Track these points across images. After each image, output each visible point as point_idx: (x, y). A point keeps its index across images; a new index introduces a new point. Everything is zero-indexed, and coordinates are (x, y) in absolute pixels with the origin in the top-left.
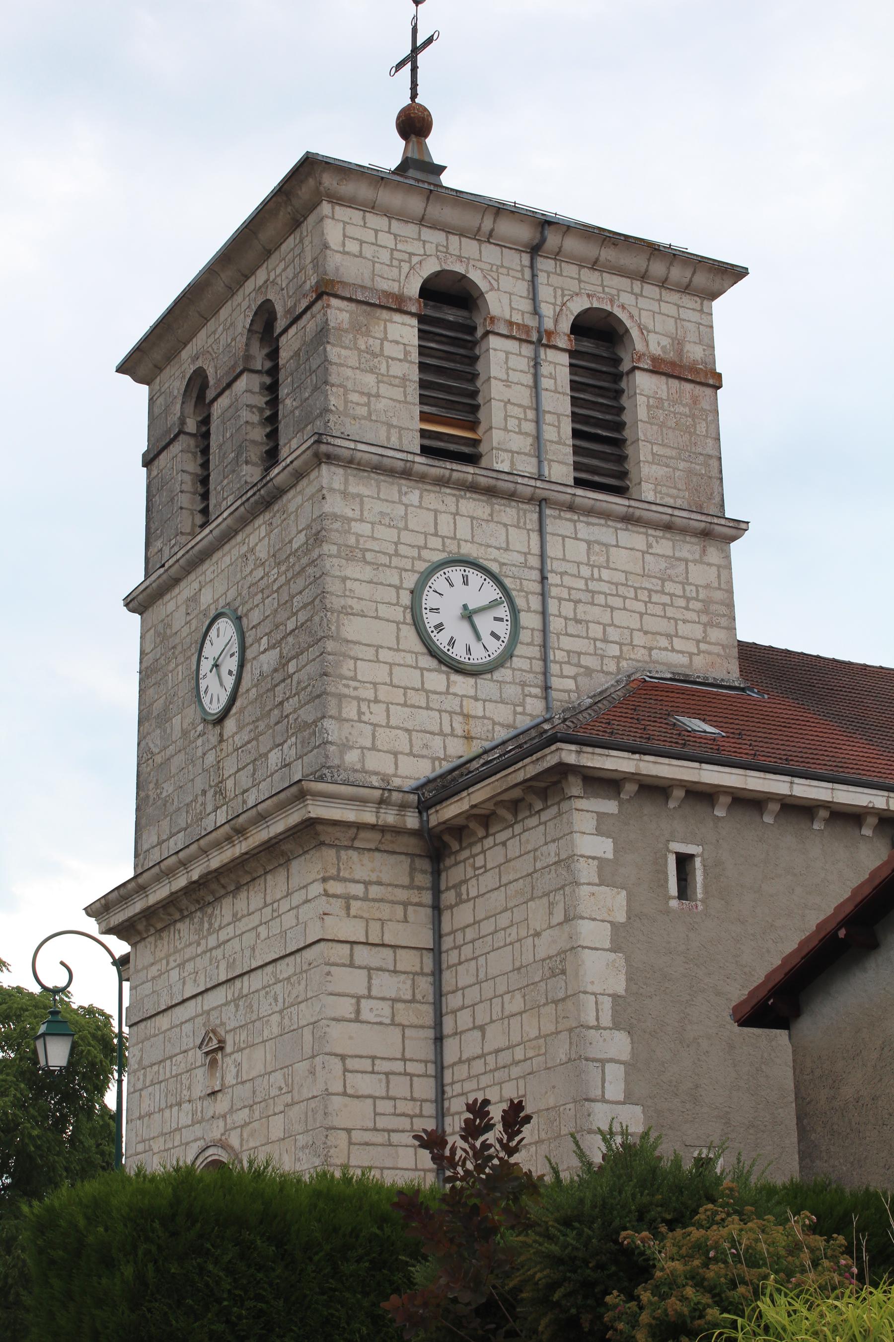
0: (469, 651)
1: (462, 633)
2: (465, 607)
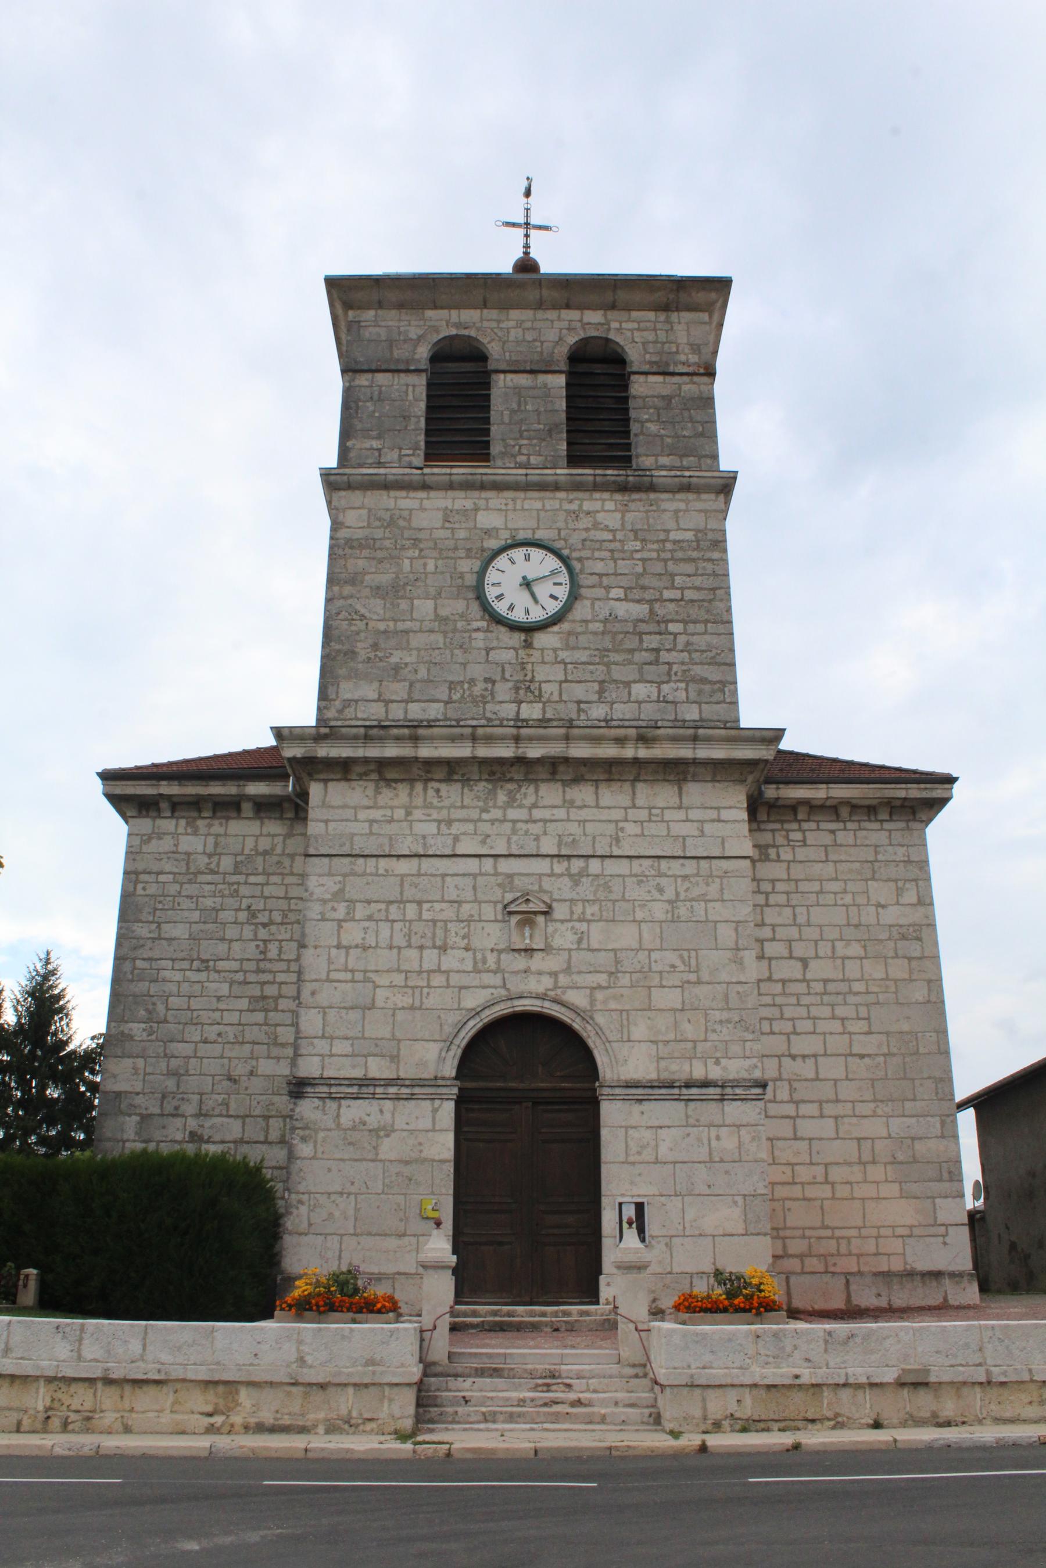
0: (527, 612)
1: (522, 599)
2: (524, 578)
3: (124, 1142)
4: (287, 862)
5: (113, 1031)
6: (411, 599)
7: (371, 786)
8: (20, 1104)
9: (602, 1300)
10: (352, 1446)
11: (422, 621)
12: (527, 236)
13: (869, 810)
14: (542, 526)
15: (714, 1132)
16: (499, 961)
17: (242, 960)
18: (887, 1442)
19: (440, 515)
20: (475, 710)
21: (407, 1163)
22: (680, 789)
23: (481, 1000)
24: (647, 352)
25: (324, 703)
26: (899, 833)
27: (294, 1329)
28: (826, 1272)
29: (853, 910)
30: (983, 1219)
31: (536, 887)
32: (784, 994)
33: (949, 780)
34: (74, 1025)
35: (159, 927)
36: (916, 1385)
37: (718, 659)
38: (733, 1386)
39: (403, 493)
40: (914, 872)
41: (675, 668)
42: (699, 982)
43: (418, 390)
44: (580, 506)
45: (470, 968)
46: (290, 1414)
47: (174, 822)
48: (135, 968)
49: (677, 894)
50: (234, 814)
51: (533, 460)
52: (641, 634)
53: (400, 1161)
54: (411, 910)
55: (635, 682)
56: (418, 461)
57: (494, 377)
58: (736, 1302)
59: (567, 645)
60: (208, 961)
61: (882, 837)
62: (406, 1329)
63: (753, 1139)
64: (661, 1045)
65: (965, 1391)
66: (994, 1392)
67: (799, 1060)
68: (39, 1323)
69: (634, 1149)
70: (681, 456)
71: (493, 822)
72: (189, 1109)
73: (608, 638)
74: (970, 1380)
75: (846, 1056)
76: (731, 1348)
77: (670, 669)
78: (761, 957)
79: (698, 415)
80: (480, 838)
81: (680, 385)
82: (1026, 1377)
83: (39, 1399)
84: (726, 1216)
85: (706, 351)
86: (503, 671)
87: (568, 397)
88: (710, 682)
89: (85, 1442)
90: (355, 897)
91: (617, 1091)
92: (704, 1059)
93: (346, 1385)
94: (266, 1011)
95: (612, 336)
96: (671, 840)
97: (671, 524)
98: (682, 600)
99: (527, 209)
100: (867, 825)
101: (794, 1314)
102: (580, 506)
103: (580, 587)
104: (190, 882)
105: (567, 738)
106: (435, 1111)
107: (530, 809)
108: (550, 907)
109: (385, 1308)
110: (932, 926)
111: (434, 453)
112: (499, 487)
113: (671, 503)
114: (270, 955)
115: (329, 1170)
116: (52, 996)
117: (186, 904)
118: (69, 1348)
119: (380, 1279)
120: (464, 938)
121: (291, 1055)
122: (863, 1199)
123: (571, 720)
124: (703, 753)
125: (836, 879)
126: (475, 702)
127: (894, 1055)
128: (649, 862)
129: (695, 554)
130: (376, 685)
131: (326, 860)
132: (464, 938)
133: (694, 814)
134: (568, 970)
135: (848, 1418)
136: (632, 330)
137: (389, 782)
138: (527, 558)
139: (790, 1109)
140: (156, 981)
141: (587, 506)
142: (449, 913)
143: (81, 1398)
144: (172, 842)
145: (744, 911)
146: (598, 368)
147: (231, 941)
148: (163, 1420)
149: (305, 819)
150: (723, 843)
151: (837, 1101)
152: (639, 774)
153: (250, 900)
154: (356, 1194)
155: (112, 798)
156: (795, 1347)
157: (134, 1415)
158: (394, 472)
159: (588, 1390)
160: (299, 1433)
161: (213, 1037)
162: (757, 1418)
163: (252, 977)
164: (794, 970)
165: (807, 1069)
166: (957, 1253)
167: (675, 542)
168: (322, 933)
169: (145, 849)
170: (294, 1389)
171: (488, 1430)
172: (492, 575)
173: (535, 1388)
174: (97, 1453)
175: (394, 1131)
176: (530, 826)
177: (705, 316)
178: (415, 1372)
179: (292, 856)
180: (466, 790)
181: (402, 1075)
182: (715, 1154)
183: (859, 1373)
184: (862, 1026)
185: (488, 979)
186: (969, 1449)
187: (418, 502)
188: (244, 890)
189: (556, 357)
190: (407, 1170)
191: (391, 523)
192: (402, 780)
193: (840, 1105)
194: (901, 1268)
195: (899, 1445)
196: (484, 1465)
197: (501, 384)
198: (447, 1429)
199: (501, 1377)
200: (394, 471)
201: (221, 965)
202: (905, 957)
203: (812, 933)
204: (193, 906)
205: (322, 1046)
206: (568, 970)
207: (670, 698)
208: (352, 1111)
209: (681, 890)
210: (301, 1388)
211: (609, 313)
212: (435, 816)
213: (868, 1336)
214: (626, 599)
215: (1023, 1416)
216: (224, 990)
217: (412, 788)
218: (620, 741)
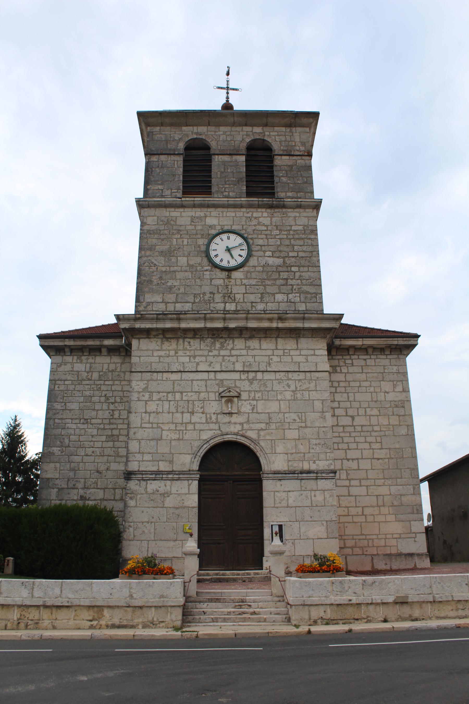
0: (229, 262)
1: (226, 257)
2: (227, 247)
3: (51, 500)
4: (122, 375)
5: (46, 451)
6: (177, 257)
7: (159, 341)
9: (264, 568)
10: (154, 634)
12: (228, 93)
13: (381, 350)
15: (313, 493)
16: (217, 419)
17: (102, 419)
18: (389, 628)
19: (189, 219)
20: (205, 306)
21: (177, 508)
22: (297, 341)
23: (209, 435)
24: (281, 145)
25: (138, 304)
26: (394, 360)
27: (127, 582)
28: (363, 554)
29: (374, 395)
30: (431, 530)
31: (233, 385)
32: (344, 432)
33: (417, 336)
34: (28, 448)
35: (65, 404)
36: (402, 603)
37: (314, 283)
38: (322, 605)
39: (173, 209)
40: (401, 377)
41: (295, 287)
42: (306, 427)
44: (252, 215)
45: (204, 422)
46: (126, 620)
47: (72, 357)
48: (55, 423)
49: (296, 388)
50: (99, 354)
51: (231, 194)
53: (174, 508)
54: (178, 396)
55: (277, 293)
56: (180, 195)
57: (213, 157)
58: (323, 568)
59: (247, 277)
60: (87, 419)
61: (387, 362)
62: (177, 582)
63: (330, 496)
64: (289, 455)
65: (424, 605)
66: (436, 606)
67: (351, 461)
70: (297, 192)
71: (214, 356)
72: (80, 485)
74: (426, 601)
75: (371, 459)
76: (321, 588)
77: (293, 288)
78: (333, 416)
80: (208, 363)
81: (296, 160)
82: (450, 599)
83: (15, 615)
84: (318, 530)
85: (308, 145)
86: (218, 289)
87: (246, 165)
89: (36, 634)
90: (153, 391)
91: (270, 475)
92: (309, 461)
93: (151, 607)
94: (114, 441)
95: (266, 138)
96: (293, 364)
97: (293, 223)
98: (297, 256)
99: (228, 81)
101: (349, 573)
102: (252, 215)
103: (252, 251)
104: (79, 384)
105: (247, 319)
106: (189, 485)
107: (230, 350)
108: (240, 394)
109: (169, 572)
110: (409, 401)
111: (188, 189)
112: (216, 206)
113: (292, 213)
115: (143, 512)
116: (18, 436)
117: (77, 394)
118: (28, 592)
119: (166, 560)
120: (201, 408)
121: (125, 461)
123: (249, 311)
124: (307, 325)
125: (367, 381)
126: (206, 303)
127: (393, 458)
128: (284, 374)
129: (303, 236)
130: (161, 295)
131: (140, 374)
132: (201, 408)
133: (304, 352)
134: (248, 422)
135: (373, 618)
136: (275, 136)
137: (167, 339)
138: (229, 238)
139: (347, 483)
141: (255, 215)
142: (195, 397)
143: (34, 614)
144: (70, 366)
145: (326, 395)
146: (260, 153)
147: (98, 410)
148: (70, 623)
149: (131, 355)
150: (316, 365)
151: (368, 479)
152: (279, 335)
154: (155, 522)
155: (42, 346)
156: (349, 587)
157: (57, 621)
158: (169, 200)
159: (258, 608)
160: (130, 628)
161: (90, 453)
162: (332, 618)
163: (107, 427)
164: (347, 421)
165: (354, 465)
166: (420, 545)
167: (294, 231)
168: (138, 406)
169: (59, 369)
170: (128, 609)
171: (214, 626)
172: (213, 246)
173: (235, 607)
175: (171, 494)
176: (230, 358)
177: (307, 129)
178: (182, 600)
179: (125, 372)
180: (202, 342)
181: (175, 469)
182: (313, 503)
183: (377, 598)
184: (378, 446)
186: (425, 630)
187: (179, 213)
188: (103, 388)
191: (168, 223)
192: (173, 338)
193: (369, 480)
195: (395, 629)
196: (213, 641)
197: (216, 160)
198: (196, 626)
199: (220, 602)
200: (169, 199)
201: (93, 421)
202: (397, 415)
203: (356, 405)
204: (81, 395)
205: (139, 457)
207: (293, 300)
208: (153, 486)
210: (131, 608)
211: (264, 128)
212: (188, 354)
214: (273, 256)
215: (449, 616)
216: (95, 432)
217: (178, 342)
218: (271, 320)
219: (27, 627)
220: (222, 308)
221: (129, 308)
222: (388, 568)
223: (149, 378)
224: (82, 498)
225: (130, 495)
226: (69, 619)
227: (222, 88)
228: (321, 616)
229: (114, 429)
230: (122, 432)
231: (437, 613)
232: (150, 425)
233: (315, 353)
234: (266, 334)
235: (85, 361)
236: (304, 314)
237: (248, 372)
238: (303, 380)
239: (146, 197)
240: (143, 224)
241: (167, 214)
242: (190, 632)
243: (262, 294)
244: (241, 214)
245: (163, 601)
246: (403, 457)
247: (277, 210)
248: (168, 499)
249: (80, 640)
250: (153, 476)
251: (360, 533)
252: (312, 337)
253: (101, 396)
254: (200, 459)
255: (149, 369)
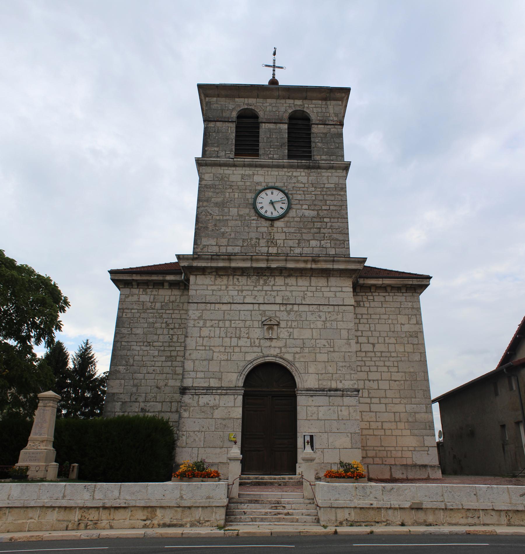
0: (272, 213)
1: (270, 209)
2: (271, 201)
3: (115, 412)
4: (181, 305)
5: (112, 370)
6: (229, 208)
7: (213, 277)
8: (74, 399)
9: (297, 473)
10: (200, 532)
11: (233, 216)
12: (274, 70)
13: (398, 289)
14: (278, 181)
15: (339, 408)
16: (260, 343)
17: (163, 342)
18: (407, 531)
19: (240, 176)
20: (252, 249)
21: (224, 419)
22: (328, 280)
23: (253, 357)
24: (318, 116)
25: (196, 246)
26: (409, 297)
27: (179, 484)
28: (383, 464)
29: (392, 326)
30: (442, 445)
31: (274, 315)
32: (366, 357)
33: (429, 278)
34: (97, 368)
35: (131, 329)
36: (418, 509)
37: (342, 232)
38: (347, 507)
39: (226, 168)
40: (415, 312)
41: (326, 235)
42: (334, 351)
43: (232, 129)
44: (292, 174)
45: (249, 345)
46: (176, 519)
47: (138, 290)
48: (121, 345)
49: (326, 318)
50: (161, 287)
51: (275, 156)
52: (314, 222)
53: (222, 419)
54: (227, 324)
55: (311, 240)
56: (232, 156)
57: (261, 124)
58: (348, 474)
59: (287, 226)
60: (150, 342)
61: (403, 299)
62: (222, 484)
63: (354, 411)
64: (320, 375)
65: (437, 512)
66: (448, 513)
67: (372, 382)
68: (78, 485)
69: (309, 414)
70: (330, 156)
71: (258, 291)
72: (141, 399)
73: (301, 224)
74: (438, 507)
75: (389, 380)
76: (345, 492)
77: (325, 235)
78: (357, 343)
79: (337, 140)
80: (253, 297)
81: (330, 129)
82: (461, 507)
83: (76, 516)
84: (344, 441)
85: (340, 116)
86: (263, 235)
87: (288, 133)
88: (339, 240)
89: (94, 533)
90: (206, 319)
91: (303, 392)
92: (336, 381)
93: (198, 507)
94: (172, 361)
95: (305, 110)
96: (324, 298)
97: (326, 182)
98: (329, 210)
99: (274, 60)
100: (398, 294)
101: (370, 480)
102: (292, 174)
103: (292, 204)
104: (144, 312)
105: (286, 260)
106: (235, 399)
107: (272, 286)
108: (279, 323)
109: (215, 476)
110: (422, 332)
111: (238, 153)
112: (262, 166)
113: (326, 173)
114: (174, 340)
115: (195, 422)
116: (89, 357)
117: (142, 321)
118: (90, 495)
119: (213, 465)
120: (247, 334)
121: (181, 378)
122: (396, 436)
123: (288, 254)
124: (336, 266)
125: (386, 314)
126: (252, 246)
127: (408, 380)
128: (316, 306)
129: (334, 193)
130: (215, 240)
131: (196, 305)
132: (247, 334)
133: (333, 289)
134: (285, 346)
135: (392, 521)
136: (313, 108)
137: (220, 276)
138: (272, 193)
139: (368, 401)
140: (130, 350)
141: (295, 174)
142: (241, 324)
143: (93, 515)
144: (137, 297)
145: (351, 325)
146: (300, 122)
147: (159, 335)
148: (126, 523)
149: (188, 289)
150: (343, 300)
151: (386, 398)
152: (312, 274)
153: (167, 319)
154: (204, 432)
155: (113, 280)
156: (371, 493)
157: (114, 521)
158: (223, 160)
159: (291, 509)
160: (180, 527)
161: (151, 371)
162: (356, 521)
163: (167, 349)
164: (370, 348)
165: (374, 385)
166: (432, 458)
167: (327, 188)
168: (193, 332)
169: (126, 300)
170: (178, 509)
171: (253, 525)
172: (259, 200)
173: (271, 508)
174: (99, 537)
175: (220, 407)
176: (272, 292)
177: (340, 103)
178: (225, 501)
179: (183, 303)
180: (248, 279)
181: (223, 385)
182: (340, 417)
183: (395, 504)
184: (395, 369)
185: (256, 349)
186: (438, 535)
187: (232, 171)
188: (165, 316)
189: (284, 117)
190: (224, 422)
191: (222, 179)
192: (225, 275)
193: (387, 399)
194: (411, 463)
195: (411, 533)
196: (252, 539)
197: (263, 127)
198: (237, 525)
199: (258, 503)
200: (223, 159)
201: (155, 344)
202: (411, 344)
203: (376, 334)
204: (145, 321)
205: (193, 374)
206: (285, 346)
207: (324, 246)
208: (204, 399)
209: (328, 317)
210: (181, 509)
211: (304, 101)
212: (237, 288)
213: (399, 488)
214: (308, 209)
215: (460, 523)
216: (156, 353)
217: (228, 279)
218: (306, 262)
219: (86, 527)
220: (266, 252)
221: (188, 249)
222: (405, 477)
223: (203, 308)
224: (143, 410)
225: (184, 408)
226: (125, 519)
227: (269, 66)
228: (346, 518)
229: (173, 350)
230: (179, 353)
231: (449, 520)
232: (204, 348)
233: (342, 290)
234: (302, 273)
235: (149, 293)
236: (334, 257)
237: (286, 304)
238: (332, 312)
239: (205, 157)
240: (201, 180)
241: (222, 172)
242: (232, 530)
243: (299, 240)
244: (283, 173)
245: (209, 502)
246: (416, 380)
247: (313, 171)
248: (216, 412)
249: (134, 538)
250: (205, 391)
251: (379, 445)
252: (340, 277)
253: (163, 323)
254: (245, 376)
255: (204, 301)
